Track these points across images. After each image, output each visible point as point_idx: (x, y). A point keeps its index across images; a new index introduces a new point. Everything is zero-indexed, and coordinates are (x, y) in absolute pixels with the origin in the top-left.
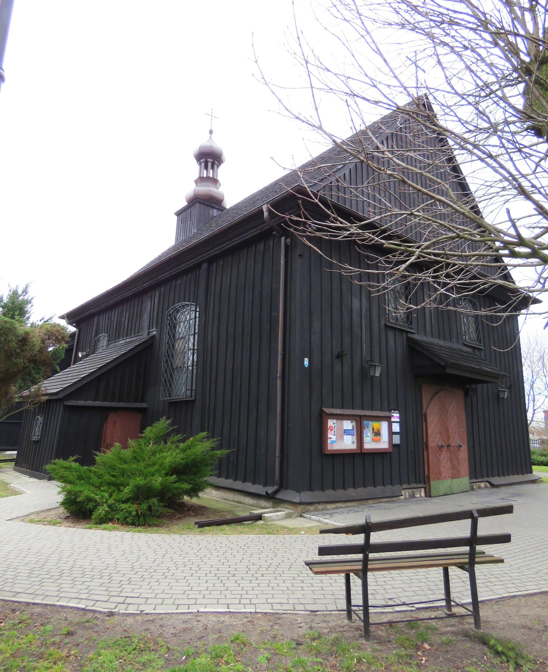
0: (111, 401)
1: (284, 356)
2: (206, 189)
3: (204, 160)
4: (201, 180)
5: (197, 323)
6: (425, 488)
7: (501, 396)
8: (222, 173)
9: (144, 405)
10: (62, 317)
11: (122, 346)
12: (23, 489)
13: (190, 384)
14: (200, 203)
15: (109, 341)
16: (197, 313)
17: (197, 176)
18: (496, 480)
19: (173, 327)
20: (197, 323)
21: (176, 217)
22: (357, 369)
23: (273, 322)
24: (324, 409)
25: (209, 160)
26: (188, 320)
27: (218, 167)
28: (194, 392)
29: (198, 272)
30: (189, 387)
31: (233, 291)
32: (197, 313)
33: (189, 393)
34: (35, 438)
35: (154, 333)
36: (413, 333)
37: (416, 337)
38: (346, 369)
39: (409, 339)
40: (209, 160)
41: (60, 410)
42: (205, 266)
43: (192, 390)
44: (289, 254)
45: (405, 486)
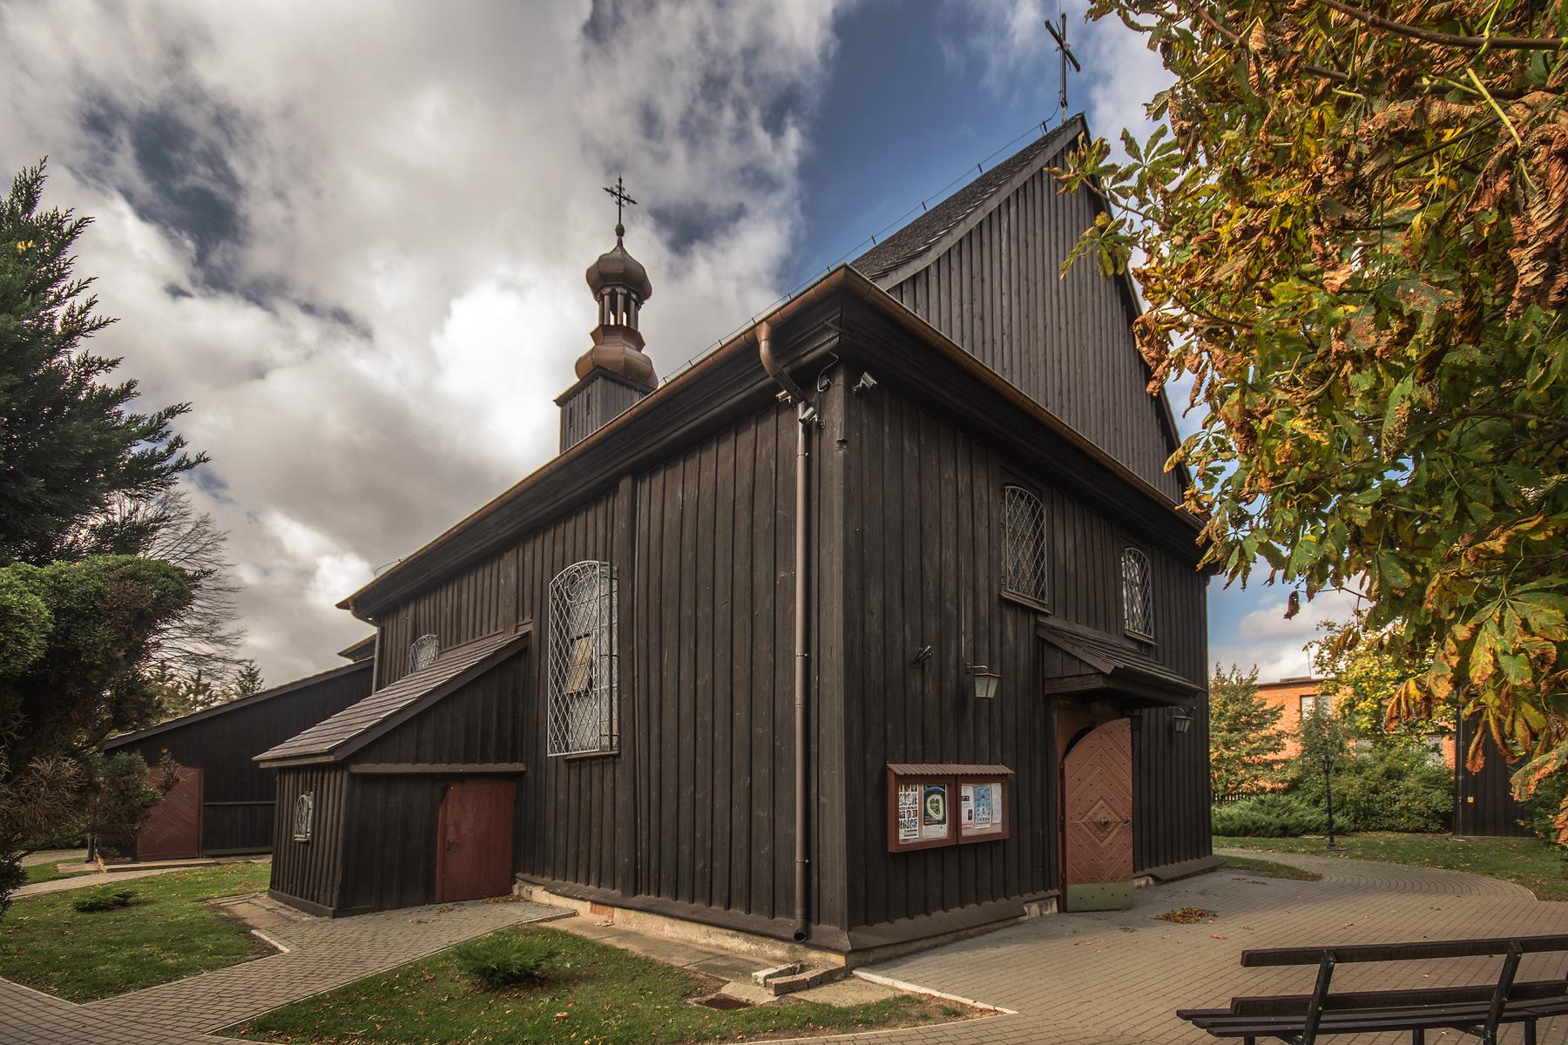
0: (450, 762)
1: (807, 663)
2: (617, 350)
3: (608, 290)
4: (603, 332)
5: (615, 602)
6: (1058, 897)
7: (1178, 727)
8: (649, 318)
9: (518, 767)
10: (340, 606)
11: (465, 658)
12: (274, 943)
13: (607, 724)
14: (605, 378)
15: (440, 648)
16: (615, 583)
17: (595, 324)
18: (1163, 870)
19: (565, 612)
20: (615, 602)
21: (559, 409)
22: (950, 685)
23: (780, 591)
24: (891, 766)
25: (619, 290)
26: (593, 605)
27: (638, 307)
28: (615, 739)
29: (609, 776)
30: (605, 731)
31: (687, 532)
32: (615, 583)
33: (606, 741)
34: (300, 838)
35: (529, 628)
36: (1045, 615)
37: (1050, 621)
38: (931, 687)
39: (1038, 625)
40: (619, 290)
41: (337, 785)
42: (625, 485)
43: (611, 736)
44: (815, 439)
45: (1026, 897)
